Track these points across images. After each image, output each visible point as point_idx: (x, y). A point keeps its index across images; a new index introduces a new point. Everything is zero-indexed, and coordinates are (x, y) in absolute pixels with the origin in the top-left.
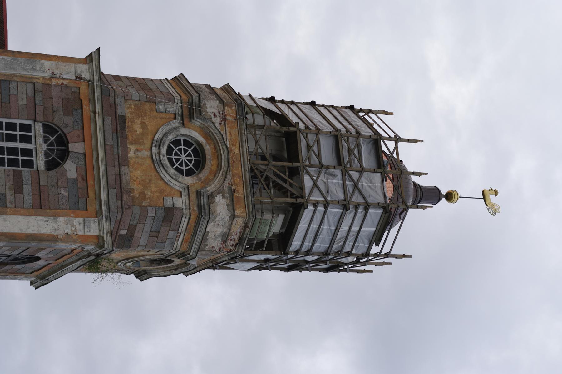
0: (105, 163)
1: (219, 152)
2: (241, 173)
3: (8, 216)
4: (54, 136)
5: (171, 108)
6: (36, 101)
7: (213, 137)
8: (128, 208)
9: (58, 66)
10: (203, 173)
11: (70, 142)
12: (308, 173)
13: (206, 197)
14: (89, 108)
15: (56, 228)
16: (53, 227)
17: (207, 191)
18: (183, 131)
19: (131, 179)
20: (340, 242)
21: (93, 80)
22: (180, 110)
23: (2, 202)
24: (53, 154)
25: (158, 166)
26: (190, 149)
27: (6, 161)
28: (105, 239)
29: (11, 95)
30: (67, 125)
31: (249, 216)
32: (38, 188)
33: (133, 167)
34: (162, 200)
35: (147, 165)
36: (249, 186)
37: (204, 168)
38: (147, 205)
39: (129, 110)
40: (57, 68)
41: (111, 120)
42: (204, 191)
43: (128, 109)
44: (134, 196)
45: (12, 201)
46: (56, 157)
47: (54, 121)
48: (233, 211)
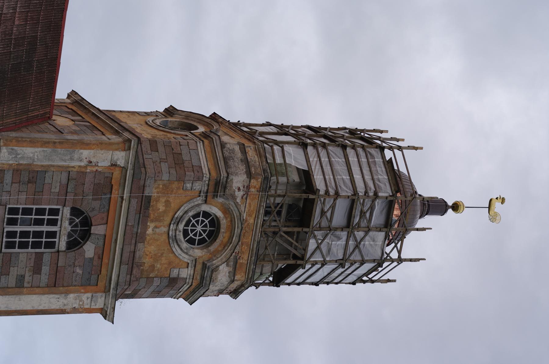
0: (122, 247)
1: (234, 226)
2: (250, 241)
3: (24, 296)
4: (80, 218)
5: (198, 186)
6: (68, 189)
7: (231, 212)
8: (135, 280)
9: (96, 154)
10: (214, 245)
11: (93, 225)
12: (315, 237)
13: (210, 270)
14: (118, 192)
15: (66, 303)
16: (63, 302)
17: (213, 265)
18: (205, 208)
19: (145, 254)
21: (127, 168)
22: (206, 188)
23: (20, 282)
24: (76, 235)
25: (172, 241)
26: (206, 235)
27: (30, 244)
28: (108, 313)
29: (45, 184)
30: (93, 209)
31: (247, 281)
32: (55, 268)
33: (148, 243)
34: (169, 271)
35: (162, 240)
36: (254, 255)
37: (215, 240)
38: (154, 276)
39: (157, 190)
40: (94, 157)
41: (137, 202)
42: (210, 264)
43: (156, 189)
44: (144, 269)
45: (29, 281)
46: (77, 237)
47: (82, 206)
48: (233, 278)
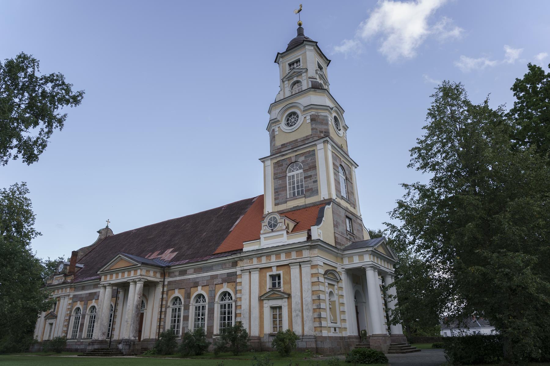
20: (393, 352)
